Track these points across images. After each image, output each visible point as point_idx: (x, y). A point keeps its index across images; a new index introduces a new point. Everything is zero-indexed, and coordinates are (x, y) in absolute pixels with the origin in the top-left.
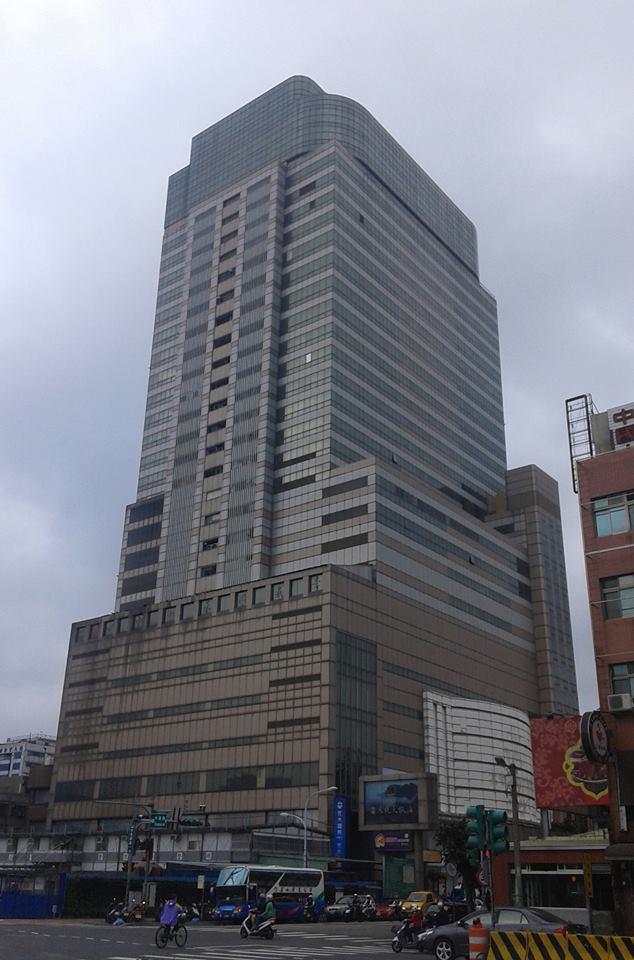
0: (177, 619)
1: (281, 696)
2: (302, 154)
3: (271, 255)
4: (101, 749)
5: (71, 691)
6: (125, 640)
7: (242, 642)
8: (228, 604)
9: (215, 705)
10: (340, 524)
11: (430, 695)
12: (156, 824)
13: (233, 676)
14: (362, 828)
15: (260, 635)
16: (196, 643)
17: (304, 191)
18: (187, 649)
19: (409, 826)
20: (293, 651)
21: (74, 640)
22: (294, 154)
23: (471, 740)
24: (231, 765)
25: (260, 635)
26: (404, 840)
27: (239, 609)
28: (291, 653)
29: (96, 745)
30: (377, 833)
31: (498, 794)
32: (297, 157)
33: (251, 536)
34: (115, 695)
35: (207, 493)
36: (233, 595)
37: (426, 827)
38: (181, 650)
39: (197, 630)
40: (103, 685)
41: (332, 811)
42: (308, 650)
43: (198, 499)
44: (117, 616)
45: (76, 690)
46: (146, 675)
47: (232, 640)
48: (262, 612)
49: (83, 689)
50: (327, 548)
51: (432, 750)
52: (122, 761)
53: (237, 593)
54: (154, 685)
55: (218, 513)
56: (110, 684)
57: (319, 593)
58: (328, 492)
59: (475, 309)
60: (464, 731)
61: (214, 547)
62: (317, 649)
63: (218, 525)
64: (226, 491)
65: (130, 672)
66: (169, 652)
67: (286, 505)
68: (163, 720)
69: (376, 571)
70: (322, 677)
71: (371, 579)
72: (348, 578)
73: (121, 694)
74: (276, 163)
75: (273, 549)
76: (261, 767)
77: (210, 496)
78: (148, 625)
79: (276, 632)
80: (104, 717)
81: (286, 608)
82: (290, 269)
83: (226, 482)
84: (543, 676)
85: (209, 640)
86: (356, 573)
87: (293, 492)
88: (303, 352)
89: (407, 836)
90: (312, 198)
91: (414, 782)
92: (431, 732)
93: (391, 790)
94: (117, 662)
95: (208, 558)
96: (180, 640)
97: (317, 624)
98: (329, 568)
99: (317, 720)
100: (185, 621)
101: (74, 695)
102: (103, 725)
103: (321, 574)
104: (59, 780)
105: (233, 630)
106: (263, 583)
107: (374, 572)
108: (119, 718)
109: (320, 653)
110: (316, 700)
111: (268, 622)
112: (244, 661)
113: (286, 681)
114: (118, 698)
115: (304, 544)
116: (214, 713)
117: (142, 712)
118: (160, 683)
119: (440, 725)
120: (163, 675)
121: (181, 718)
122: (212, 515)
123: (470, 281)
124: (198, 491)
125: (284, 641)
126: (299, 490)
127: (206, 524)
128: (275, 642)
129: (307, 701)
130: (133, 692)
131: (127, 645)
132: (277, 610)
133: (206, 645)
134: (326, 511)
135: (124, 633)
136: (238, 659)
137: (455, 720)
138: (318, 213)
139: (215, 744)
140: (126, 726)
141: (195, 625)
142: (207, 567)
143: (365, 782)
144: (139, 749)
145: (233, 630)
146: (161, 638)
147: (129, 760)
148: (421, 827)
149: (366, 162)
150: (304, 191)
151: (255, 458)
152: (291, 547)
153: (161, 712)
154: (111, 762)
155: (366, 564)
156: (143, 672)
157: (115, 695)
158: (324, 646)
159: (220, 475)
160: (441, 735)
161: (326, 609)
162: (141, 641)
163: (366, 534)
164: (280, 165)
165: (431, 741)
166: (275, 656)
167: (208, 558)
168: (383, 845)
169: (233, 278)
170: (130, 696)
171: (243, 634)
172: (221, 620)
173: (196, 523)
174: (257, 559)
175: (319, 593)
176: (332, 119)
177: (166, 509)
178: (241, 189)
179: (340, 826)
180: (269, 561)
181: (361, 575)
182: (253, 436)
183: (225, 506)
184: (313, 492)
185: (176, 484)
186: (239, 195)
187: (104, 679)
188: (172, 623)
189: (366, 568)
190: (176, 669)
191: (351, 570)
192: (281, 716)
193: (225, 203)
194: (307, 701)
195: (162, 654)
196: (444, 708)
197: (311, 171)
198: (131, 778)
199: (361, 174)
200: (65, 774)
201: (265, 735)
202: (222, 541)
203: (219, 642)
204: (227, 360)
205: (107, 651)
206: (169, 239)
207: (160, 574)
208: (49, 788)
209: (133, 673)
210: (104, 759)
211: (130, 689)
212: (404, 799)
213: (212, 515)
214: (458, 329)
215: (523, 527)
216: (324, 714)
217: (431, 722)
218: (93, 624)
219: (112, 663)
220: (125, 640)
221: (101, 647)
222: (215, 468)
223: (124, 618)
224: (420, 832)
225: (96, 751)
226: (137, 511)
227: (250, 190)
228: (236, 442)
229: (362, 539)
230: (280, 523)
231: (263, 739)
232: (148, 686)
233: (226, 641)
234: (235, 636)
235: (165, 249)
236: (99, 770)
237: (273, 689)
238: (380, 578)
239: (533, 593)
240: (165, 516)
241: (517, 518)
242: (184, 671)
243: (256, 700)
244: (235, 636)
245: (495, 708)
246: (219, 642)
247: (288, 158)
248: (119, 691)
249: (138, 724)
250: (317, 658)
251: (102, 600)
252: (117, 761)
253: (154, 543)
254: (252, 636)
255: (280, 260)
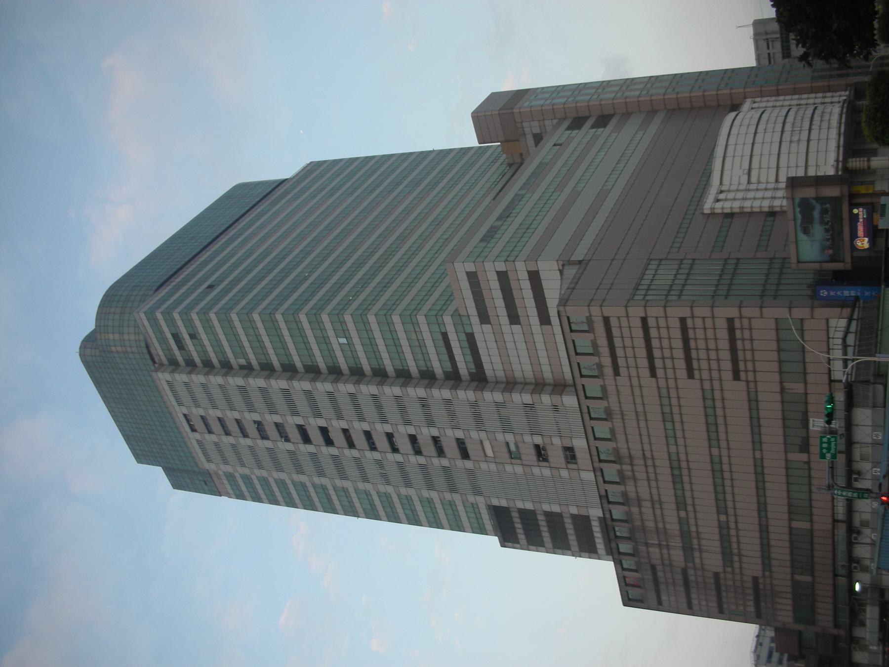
0: (620, 488)
1: (704, 365)
2: (147, 347)
3: (240, 381)
4: (759, 574)
5: (695, 607)
6: (642, 548)
7: (645, 412)
8: (602, 430)
9: (714, 443)
10: (518, 303)
11: (707, 206)
12: (833, 451)
13: (682, 422)
14: (849, 266)
15: (637, 391)
16: (646, 466)
17: (181, 346)
18: (652, 476)
19: (845, 208)
20: (653, 340)
21: (641, 604)
22: (147, 356)
23: (755, 165)
24: (780, 423)
25: (637, 391)
26: (861, 213)
27: (608, 415)
28: (657, 353)
29: (755, 580)
30: (853, 248)
31: (812, 138)
32: (150, 353)
33: (531, 406)
34: (701, 558)
35: (486, 456)
36: (593, 423)
37: (846, 188)
38: (653, 484)
39: (632, 465)
40: (691, 572)
41: (830, 303)
42: (653, 333)
43: (493, 467)
44: (616, 556)
45: (695, 602)
46: (680, 523)
47: (642, 424)
48: (611, 389)
49: (694, 596)
50: (545, 319)
51: (766, 204)
52: (773, 550)
53: (591, 419)
54: (691, 515)
55: (507, 444)
56: (690, 565)
57: (589, 321)
58: (484, 318)
59: (315, 180)
60: (746, 171)
61: (544, 449)
62: (651, 322)
63: (520, 445)
64: (483, 435)
65: (676, 542)
66: (656, 497)
67: (498, 367)
68: (730, 504)
69: (569, 261)
70: (755, 575)
71: (578, 267)
72: (574, 288)
73: (701, 551)
74: (154, 374)
75: (547, 381)
76: (783, 391)
77: (489, 453)
78: (626, 521)
79: (633, 372)
80: (724, 572)
81: (606, 361)
82: (254, 363)
83: (474, 434)
84: (691, 102)
85: (643, 450)
86: (569, 281)
87: (484, 359)
88: (336, 347)
89: (855, 211)
90: (186, 336)
91: (797, 201)
92: (747, 204)
93: (806, 231)
94: (666, 557)
95: (556, 456)
96: (643, 484)
97: (624, 322)
98: (561, 308)
99: (730, 321)
100: (622, 479)
101: (700, 604)
102: (733, 572)
103: (568, 318)
104: (790, 620)
105: (631, 422)
106: (580, 388)
107: (570, 263)
108: (727, 554)
109: (657, 318)
110: (709, 322)
111: (622, 380)
112: (667, 409)
113: (688, 359)
114: (705, 555)
115: (540, 346)
116: (723, 444)
117: (720, 527)
118: (690, 508)
119: (740, 195)
120: (681, 504)
121: (728, 483)
122: (510, 452)
123: (288, 185)
124: (484, 466)
125: (644, 363)
126: (483, 352)
127: (520, 458)
128: (645, 372)
129: (710, 334)
130: (699, 538)
131: (647, 545)
132: (609, 371)
133: (648, 454)
134: (504, 320)
135: (635, 549)
136: (663, 417)
137: (735, 181)
138: (201, 330)
139: (757, 443)
140: (735, 546)
141: (627, 468)
142: (566, 457)
143: (799, 262)
144: (761, 531)
145: (631, 422)
146: (640, 506)
147: (772, 543)
148: (846, 193)
149: (158, 284)
150: (181, 346)
151: (448, 402)
152: (544, 360)
153: (721, 508)
154: (774, 562)
155: (561, 272)
156: (677, 527)
157: (701, 558)
158: (649, 314)
159: (467, 441)
160: (751, 195)
161: (607, 312)
162: (644, 528)
163: (529, 273)
164: (157, 370)
165: (757, 204)
166: (660, 373)
167: (556, 456)
168: (866, 239)
169: (264, 423)
170: (703, 542)
171: (636, 412)
172: (621, 437)
173: (519, 469)
174: (556, 399)
175: (589, 321)
176: (117, 317)
177: (504, 503)
178: (179, 412)
179: (846, 293)
180: (559, 387)
181: (572, 277)
182: (424, 404)
183: (500, 437)
184: (483, 335)
185: (477, 492)
186: (185, 415)
187: (684, 572)
188: (625, 494)
189: (566, 271)
190: (675, 489)
191: (565, 286)
192: (727, 365)
193: (193, 430)
194: (710, 334)
195: (657, 506)
196: (721, 192)
197: (162, 340)
198: (791, 541)
199: (169, 288)
200: (785, 614)
201: (748, 382)
202: (538, 440)
203: (645, 439)
204: (345, 431)
205: (653, 568)
206: (230, 491)
207: (574, 510)
208: (800, 632)
209: (678, 539)
210: (770, 571)
211: (695, 541)
212: (816, 214)
213: (510, 452)
214: (332, 195)
215: (536, 124)
216: (724, 312)
217: (737, 204)
218: (625, 584)
219: (667, 562)
220: (642, 548)
221: (648, 576)
222: (459, 447)
223: (618, 548)
224: (852, 196)
225: (761, 580)
226: (508, 538)
227: (180, 404)
228: (431, 423)
229: (535, 277)
230: (518, 375)
231: (752, 385)
232: (692, 521)
233: (644, 432)
234: (638, 420)
235: (241, 496)
236: (782, 576)
237: (696, 374)
238: (576, 257)
239: (606, 113)
240: (511, 504)
241: (527, 130)
242: (677, 479)
243: (708, 395)
244: (638, 420)
245: (722, 141)
246: (645, 439)
247: (150, 362)
248: (697, 554)
249: (733, 532)
250: (662, 323)
251: (600, 575)
252: (773, 555)
253: (541, 517)
254: (638, 400)
255: (245, 372)
